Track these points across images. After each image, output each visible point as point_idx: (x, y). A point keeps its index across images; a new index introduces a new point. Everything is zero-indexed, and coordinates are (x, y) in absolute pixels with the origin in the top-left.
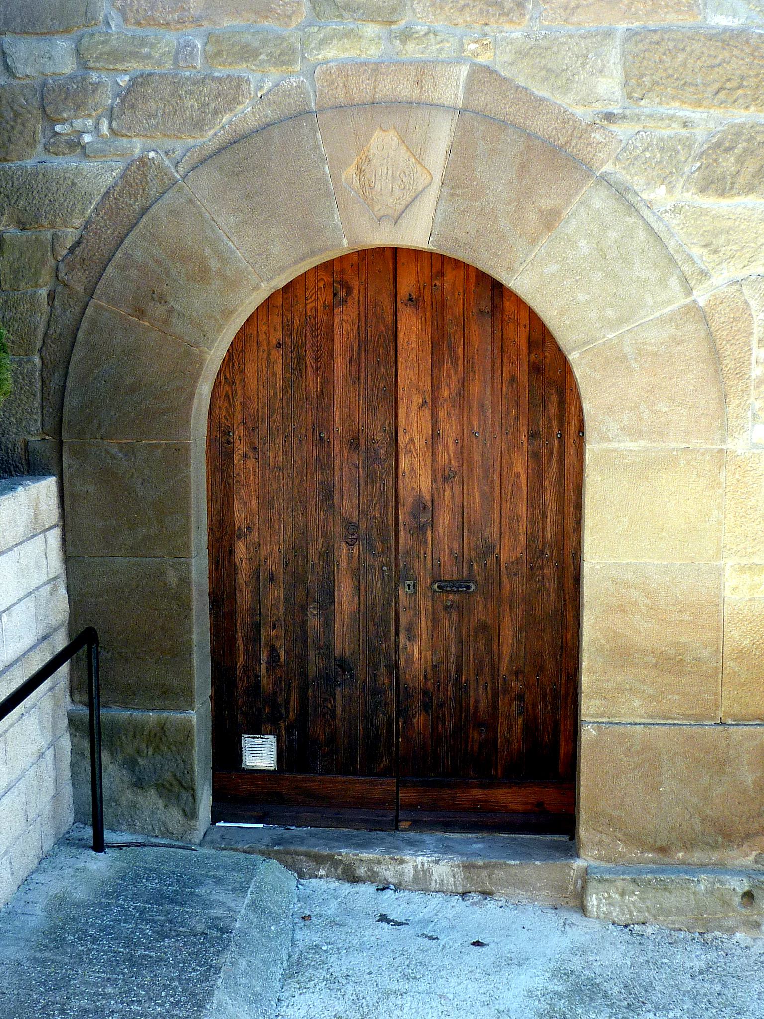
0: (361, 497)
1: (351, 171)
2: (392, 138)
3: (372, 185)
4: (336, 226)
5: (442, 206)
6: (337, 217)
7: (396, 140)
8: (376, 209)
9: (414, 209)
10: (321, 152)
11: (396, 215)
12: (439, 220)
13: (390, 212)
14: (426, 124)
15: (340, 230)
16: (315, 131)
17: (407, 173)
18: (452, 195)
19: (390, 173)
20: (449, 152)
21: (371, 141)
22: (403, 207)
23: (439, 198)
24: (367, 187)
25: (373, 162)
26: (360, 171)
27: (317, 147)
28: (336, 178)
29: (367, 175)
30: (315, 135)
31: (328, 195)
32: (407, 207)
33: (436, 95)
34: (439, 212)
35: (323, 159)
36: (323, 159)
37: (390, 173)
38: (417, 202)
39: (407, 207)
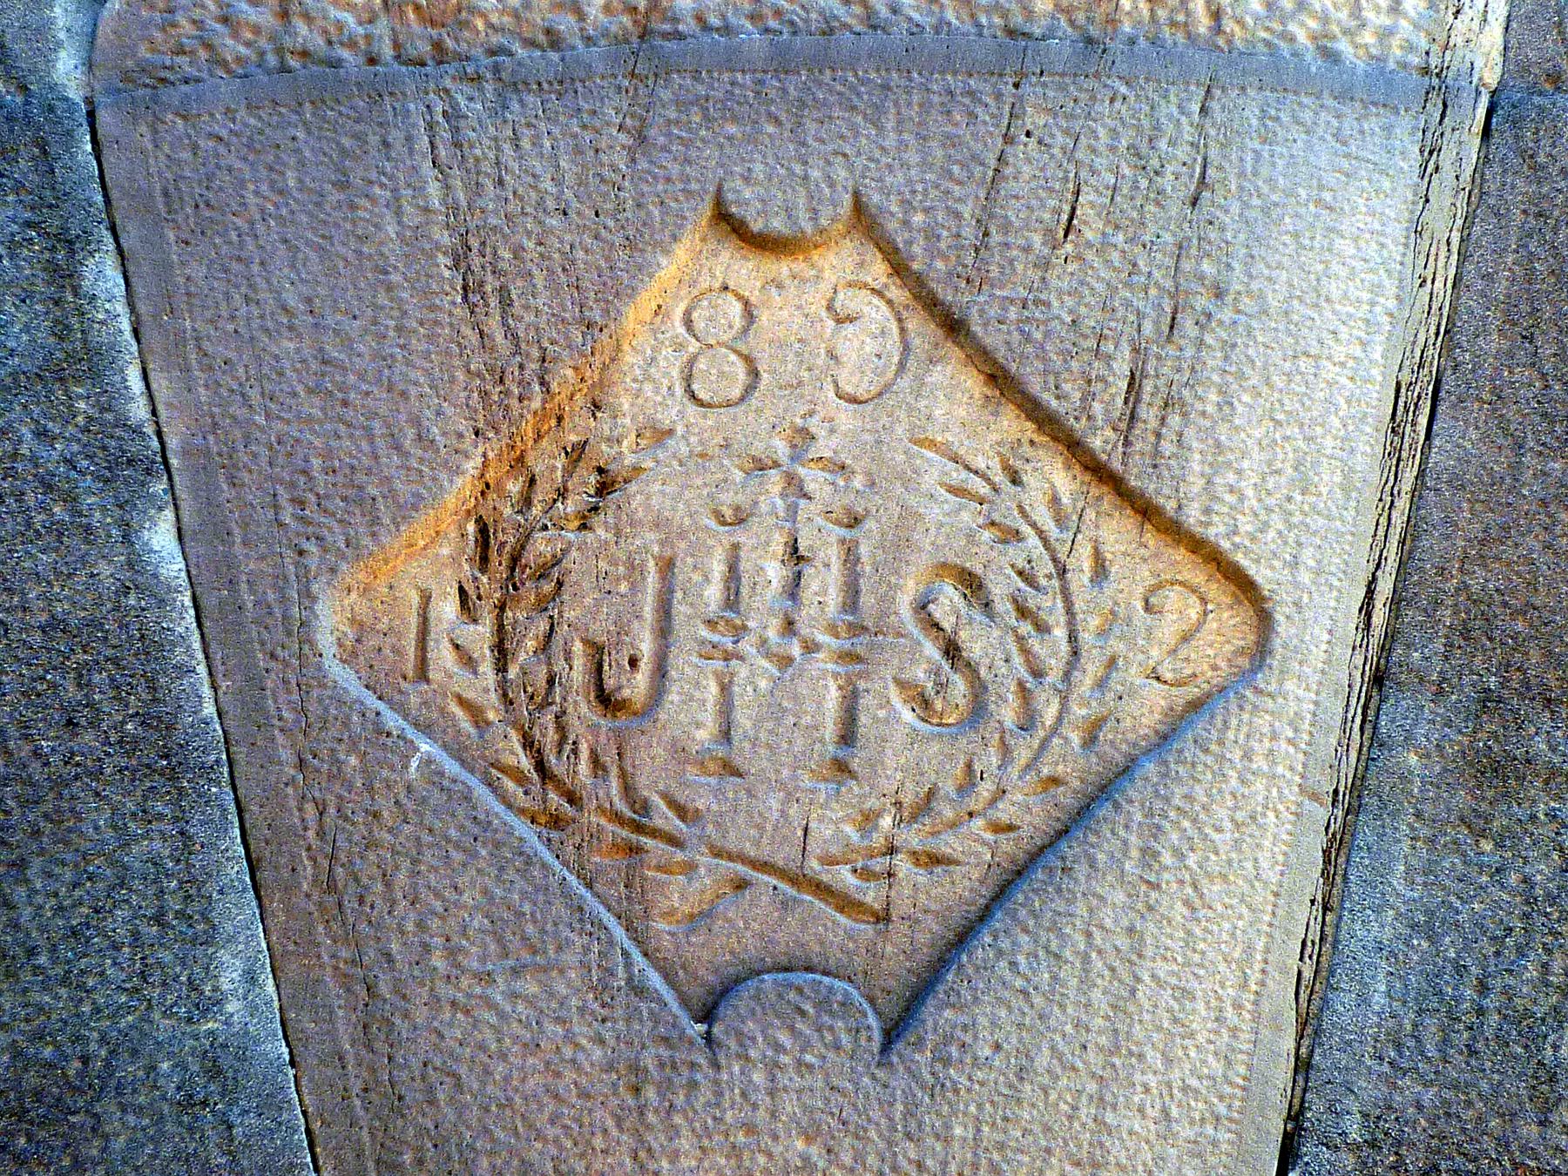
0: (213, 646)
1: (421, 571)
2: (834, 317)
3: (637, 686)
4: (221, 1066)
5: (1397, 866)
6: (241, 978)
7: (873, 329)
8: (678, 896)
9: (1100, 895)
10: (110, 399)
11: (899, 953)
12: (1370, 1000)
13: (835, 931)
14: (1177, 186)
15: (271, 1102)
16: (71, 244)
17: (1000, 587)
18: (1496, 771)
19: (824, 587)
20: (1429, 393)
21: (635, 314)
22: (963, 886)
23: (1353, 800)
24: (582, 709)
25: (648, 496)
26: (506, 565)
27: (77, 361)
28: (252, 621)
29: (581, 610)
30: (64, 276)
31: (163, 759)
32: (1001, 893)
33: (1076, 784)
34: (1369, 929)
35: (128, 466)
36: (128, 466)
37: (824, 587)
38: (1116, 837)
39: (1001, 893)
